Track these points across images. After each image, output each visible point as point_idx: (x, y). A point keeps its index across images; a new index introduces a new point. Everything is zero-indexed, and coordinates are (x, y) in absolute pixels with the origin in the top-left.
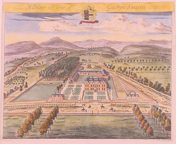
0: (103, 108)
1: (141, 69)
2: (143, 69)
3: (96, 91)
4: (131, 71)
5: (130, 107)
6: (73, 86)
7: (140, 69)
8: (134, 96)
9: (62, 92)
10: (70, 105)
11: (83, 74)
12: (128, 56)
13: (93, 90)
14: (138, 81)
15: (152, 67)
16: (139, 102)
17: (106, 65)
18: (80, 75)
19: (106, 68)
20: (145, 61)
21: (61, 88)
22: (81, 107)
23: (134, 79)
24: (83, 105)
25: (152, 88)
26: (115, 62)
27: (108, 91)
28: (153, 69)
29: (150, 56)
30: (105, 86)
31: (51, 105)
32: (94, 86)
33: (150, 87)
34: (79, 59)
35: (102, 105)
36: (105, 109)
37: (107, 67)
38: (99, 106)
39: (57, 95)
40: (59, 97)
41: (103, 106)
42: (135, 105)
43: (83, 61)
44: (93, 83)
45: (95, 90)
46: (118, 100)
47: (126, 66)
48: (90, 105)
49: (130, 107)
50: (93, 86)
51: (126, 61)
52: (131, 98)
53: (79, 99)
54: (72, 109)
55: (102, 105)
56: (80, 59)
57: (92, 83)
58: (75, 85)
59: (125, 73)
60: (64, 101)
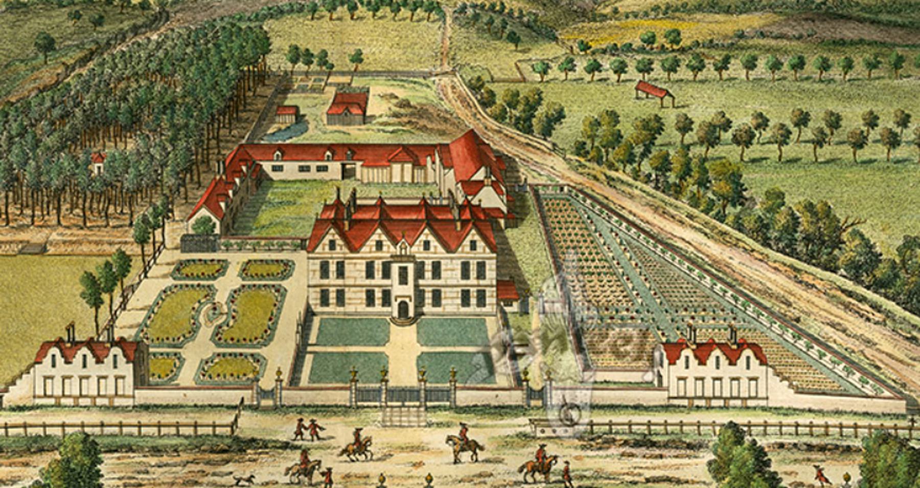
0: (466, 456)
1: (784, 137)
2: (795, 131)
3: (411, 313)
4: (697, 151)
5: (690, 446)
6: (222, 268)
7: (767, 134)
8: (723, 359)
9: (124, 319)
10: (189, 431)
11: (302, 169)
12: (668, 25)
13: (386, 301)
14: (761, 232)
15: (872, 121)
16: (764, 409)
17: (492, 94)
18: (275, 176)
19: (493, 124)
20: (811, 68)
21: (117, 291)
22: (286, 446)
23: (721, 218)
24: (299, 433)
25: (869, 294)
26: (562, 76)
27: (507, 309)
28: (874, 134)
29: (849, 32)
30: (481, 275)
31: (40, 431)
32: (395, 268)
33: (857, 280)
34: (264, 45)
35: (465, 428)
36: (487, 461)
37: (500, 117)
38: (437, 438)
39: (85, 350)
40: (99, 361)
41: (470, 436)
42: (736, 432)
43: (301, 66)
44: (387, 243)
45: (403, 307)
46: (598, 386)
47: (649, 107)
48: (357, 433)
49: (690, 446)
50: (386, 274)
51: (656, 66)
52: (701, 371)
53: (267, 383)
54: (208, 463)
55: (465, 428)
56: (276, 43)
57: (379, 245)
58: (236, 259)
59: (646, 167)
60: (145, 396)
